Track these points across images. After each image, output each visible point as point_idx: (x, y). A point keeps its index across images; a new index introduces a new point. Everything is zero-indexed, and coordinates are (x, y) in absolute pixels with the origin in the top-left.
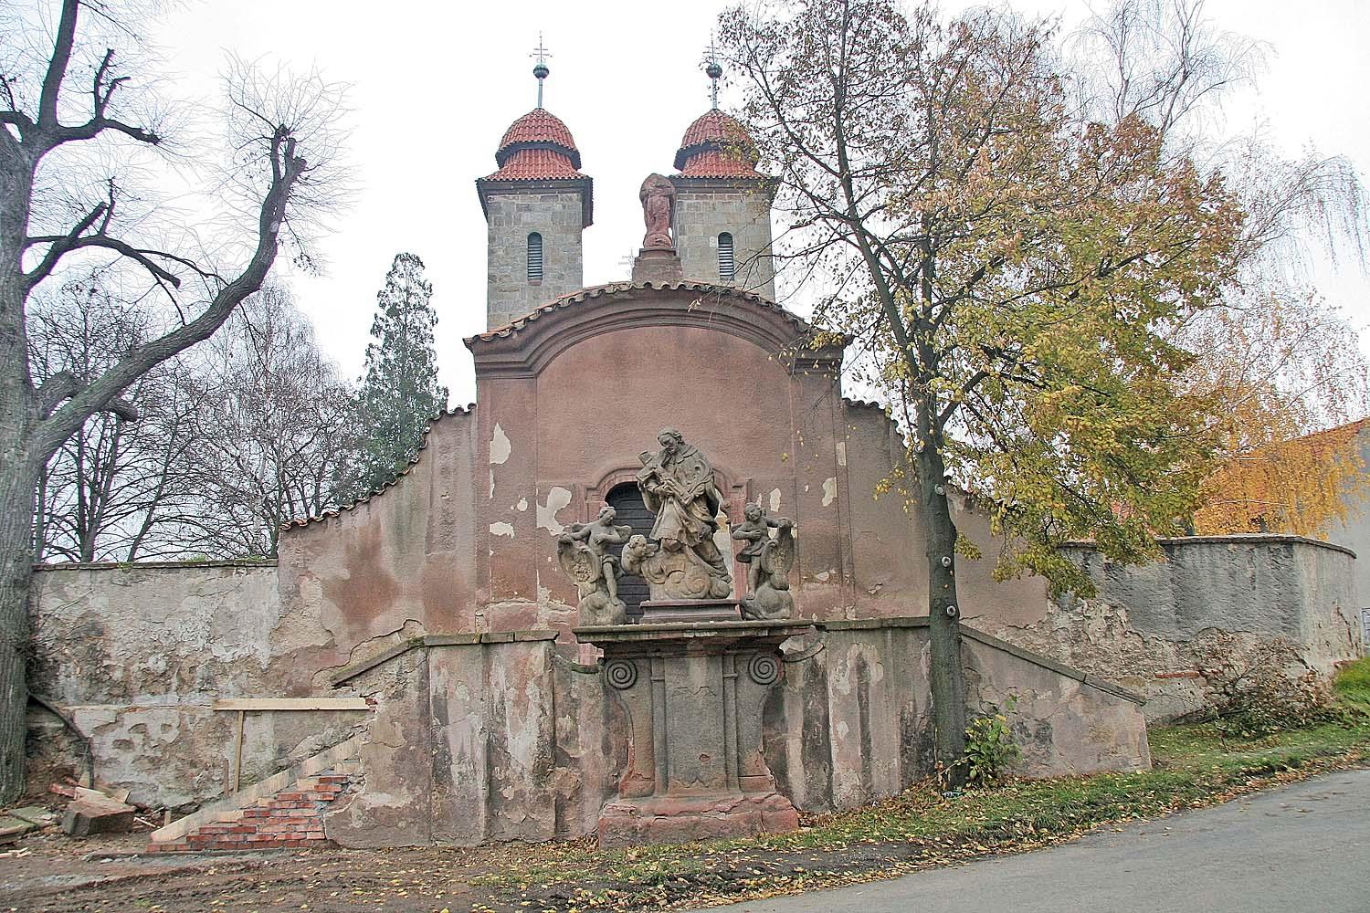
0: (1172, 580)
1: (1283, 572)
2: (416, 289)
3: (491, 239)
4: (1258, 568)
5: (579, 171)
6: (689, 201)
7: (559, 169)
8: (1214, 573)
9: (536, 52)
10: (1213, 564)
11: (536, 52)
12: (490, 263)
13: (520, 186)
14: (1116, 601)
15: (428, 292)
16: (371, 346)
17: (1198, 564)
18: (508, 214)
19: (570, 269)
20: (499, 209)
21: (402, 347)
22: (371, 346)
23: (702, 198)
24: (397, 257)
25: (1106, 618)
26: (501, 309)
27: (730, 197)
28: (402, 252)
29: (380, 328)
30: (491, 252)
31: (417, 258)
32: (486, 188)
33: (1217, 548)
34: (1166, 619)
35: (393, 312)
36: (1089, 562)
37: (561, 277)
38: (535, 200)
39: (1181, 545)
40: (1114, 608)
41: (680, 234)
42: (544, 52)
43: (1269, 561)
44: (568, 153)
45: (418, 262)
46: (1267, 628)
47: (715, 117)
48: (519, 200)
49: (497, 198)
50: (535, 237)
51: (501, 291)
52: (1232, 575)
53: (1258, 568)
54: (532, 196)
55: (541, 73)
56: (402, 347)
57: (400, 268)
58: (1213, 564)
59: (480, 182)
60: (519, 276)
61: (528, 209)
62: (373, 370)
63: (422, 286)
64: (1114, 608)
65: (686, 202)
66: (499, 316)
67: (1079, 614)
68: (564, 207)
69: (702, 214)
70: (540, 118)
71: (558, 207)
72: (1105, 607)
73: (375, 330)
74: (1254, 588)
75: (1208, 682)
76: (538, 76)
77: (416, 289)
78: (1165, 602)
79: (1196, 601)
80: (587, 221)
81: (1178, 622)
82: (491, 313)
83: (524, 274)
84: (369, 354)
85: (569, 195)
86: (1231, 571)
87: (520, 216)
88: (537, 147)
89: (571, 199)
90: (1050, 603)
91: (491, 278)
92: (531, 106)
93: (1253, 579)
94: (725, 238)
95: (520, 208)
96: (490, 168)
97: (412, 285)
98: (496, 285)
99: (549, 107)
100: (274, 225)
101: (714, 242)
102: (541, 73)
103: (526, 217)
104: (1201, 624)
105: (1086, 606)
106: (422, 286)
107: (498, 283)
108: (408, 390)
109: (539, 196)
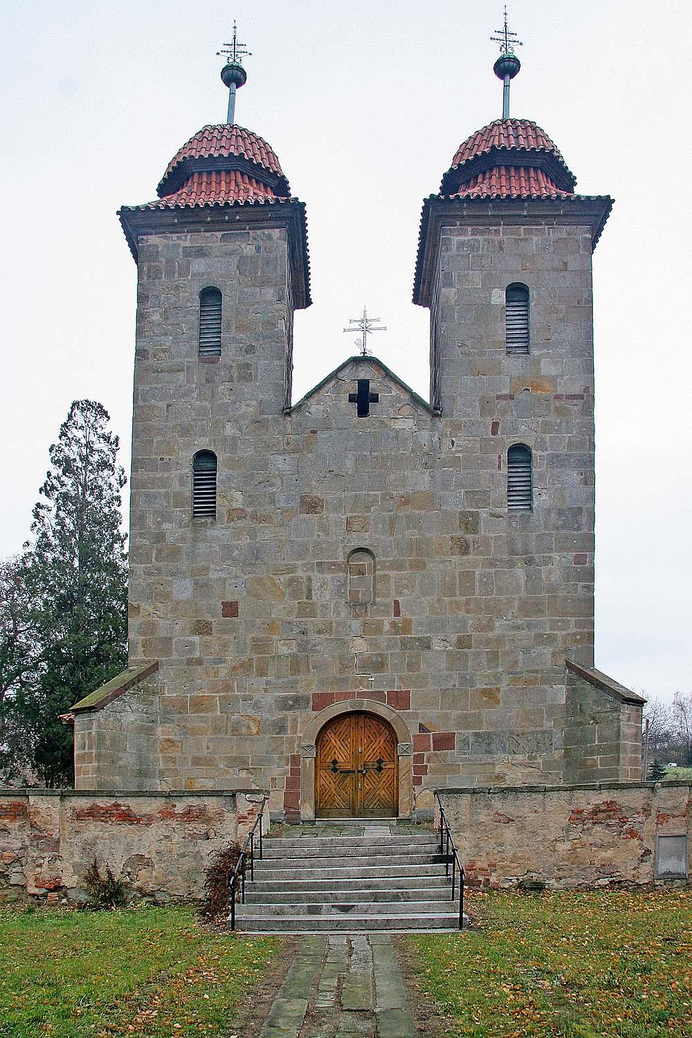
2: (100, 445)
3: (142, 298)
5: (291, 197)
6: (462, 238)
7: (256, 194)
9: (227, 48)
11: (227, 48)
12: (139, 333)
13: (189, 218)
15: (114, 446)
16: (38, 505)
18: (170, 262)
19: (265, 338)
20: (155, 255)
21: (81, 508)
22: (38, 505)
23: (482, 233)
24: (74, 404)
26: (154, 397)
27: (527, 232)
28: (80, 398)
29: (53, 488)
30: (141, 317)
31: (100, 406)
35: (67, 466)
37: (250, 349)
38: (212, 240)
41: (444, 287)
42: (239, 49)
44: (269, 181)
45: (102, 412)
47: (505, 124)
48: (186, 241)
49: (154, 240)
50: (211, 295)
51: (157, 371)
54: (207, 234)
56: (81, 508)
57: (79, 418)
59: (126, 214)
60: (185, 349)
61: (201, 253)
62: (44, 535)
63: (106, 438)
65: (456, 239)
66: (152, 408)
68: (258, 249)
69: (481, 257)
71: (248, 249)
73: (47, 490)
76: (227, 82)
77: (100, 445)
80: (302, 298)
82: (141, 403)
83: (192, 347)
84: (37, 515)
85: (266, 232)
87: (189, 263)
88: (220, 166)
89: (270, 238)
91: (140, 354)
94: (517, 292)
95: (188, 253)
96: (145, 194)
97: (94, 439)
98: (147, 363)
101: (499, 297)
103: (198, 265)
106: (106, 438)
107: (151, 361)
108: (90, 558)
109: (219, 234)
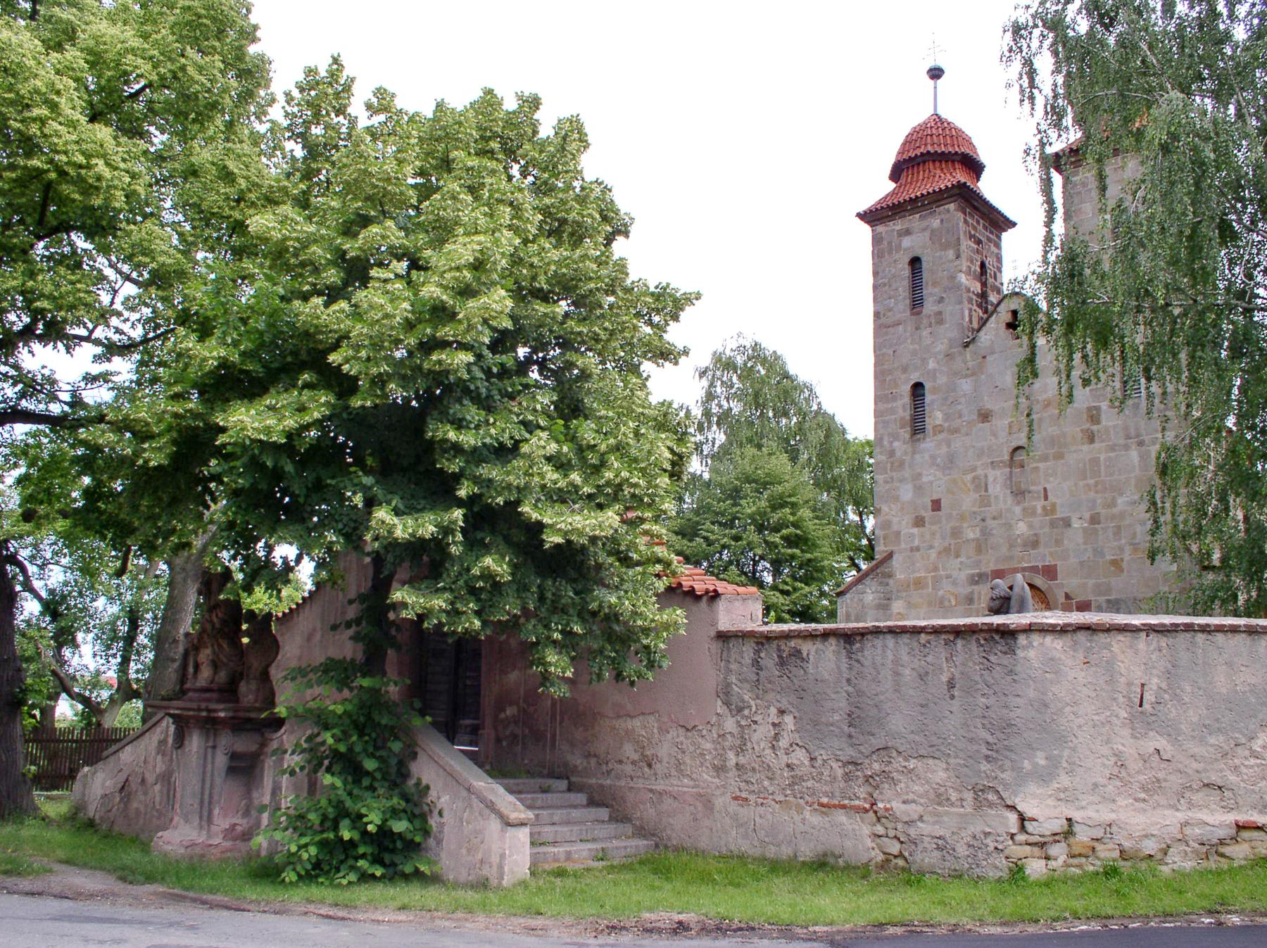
0: (848, 680)
1: (997, 676)
4: (960, 668)
8: (897, 674)
10: (896, 662)
14: (784, 704)
17: (878, 659)
18: (890, 243)
25: (774, 725)
32: (871, 217)
33: (905, 639)
34: (837, 731)
36: (762, 655)
38: (914, 221)
39: (863, 635)
40: (782, 712)
43: (977, 658)
46: (961, 754)
50: (915, 262)
52: (922, 677)
53: (960, 668)
55: (936, 73)
58: (896, 662)
61: (908, 232)
64: (782, 712)
67: (747, 717)
70: (938, 127)
71: (935, 223)
72: (773, 710)
74: (952, 697)
75: (879, 819)
78: (838, 705)
79: (873, 713)
81: (850, 736)
86: (922, 671)
89: (948, 211)
90: (719, 702)
91: (877, 315)
92: (920, 115)
93: (951, 684)
99: (944, 114)
100: (283, 376)
102: (936, 73)
103: (906, 242)
104: (877, 742)
105: (754, 709)
